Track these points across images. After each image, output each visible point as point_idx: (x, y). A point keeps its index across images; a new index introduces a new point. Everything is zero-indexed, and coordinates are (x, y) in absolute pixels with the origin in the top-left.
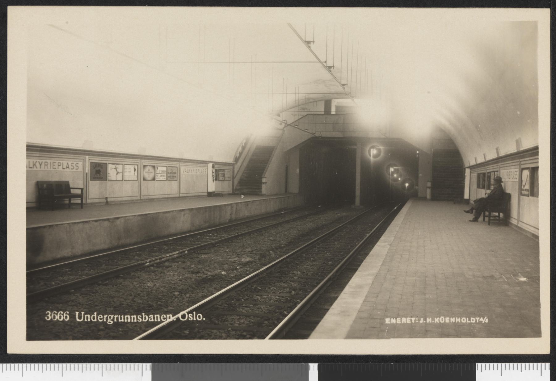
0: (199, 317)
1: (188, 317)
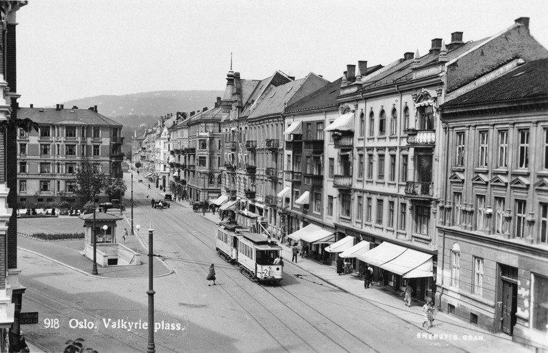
0: (90, 325)
1: (79, 325)
